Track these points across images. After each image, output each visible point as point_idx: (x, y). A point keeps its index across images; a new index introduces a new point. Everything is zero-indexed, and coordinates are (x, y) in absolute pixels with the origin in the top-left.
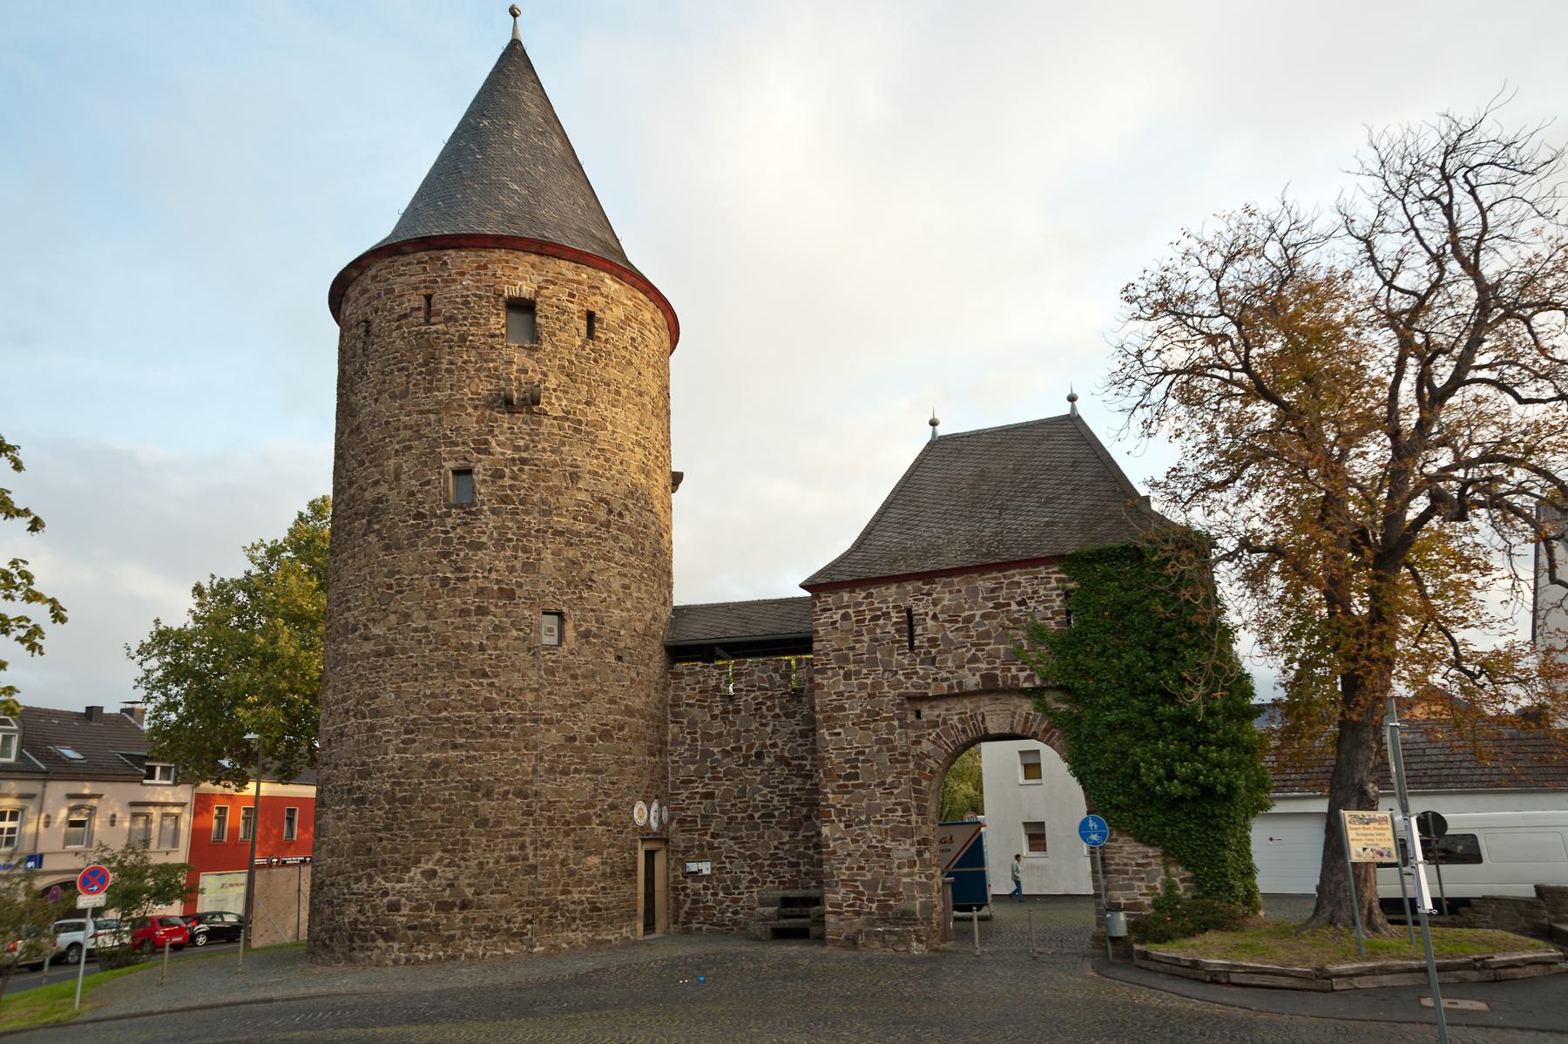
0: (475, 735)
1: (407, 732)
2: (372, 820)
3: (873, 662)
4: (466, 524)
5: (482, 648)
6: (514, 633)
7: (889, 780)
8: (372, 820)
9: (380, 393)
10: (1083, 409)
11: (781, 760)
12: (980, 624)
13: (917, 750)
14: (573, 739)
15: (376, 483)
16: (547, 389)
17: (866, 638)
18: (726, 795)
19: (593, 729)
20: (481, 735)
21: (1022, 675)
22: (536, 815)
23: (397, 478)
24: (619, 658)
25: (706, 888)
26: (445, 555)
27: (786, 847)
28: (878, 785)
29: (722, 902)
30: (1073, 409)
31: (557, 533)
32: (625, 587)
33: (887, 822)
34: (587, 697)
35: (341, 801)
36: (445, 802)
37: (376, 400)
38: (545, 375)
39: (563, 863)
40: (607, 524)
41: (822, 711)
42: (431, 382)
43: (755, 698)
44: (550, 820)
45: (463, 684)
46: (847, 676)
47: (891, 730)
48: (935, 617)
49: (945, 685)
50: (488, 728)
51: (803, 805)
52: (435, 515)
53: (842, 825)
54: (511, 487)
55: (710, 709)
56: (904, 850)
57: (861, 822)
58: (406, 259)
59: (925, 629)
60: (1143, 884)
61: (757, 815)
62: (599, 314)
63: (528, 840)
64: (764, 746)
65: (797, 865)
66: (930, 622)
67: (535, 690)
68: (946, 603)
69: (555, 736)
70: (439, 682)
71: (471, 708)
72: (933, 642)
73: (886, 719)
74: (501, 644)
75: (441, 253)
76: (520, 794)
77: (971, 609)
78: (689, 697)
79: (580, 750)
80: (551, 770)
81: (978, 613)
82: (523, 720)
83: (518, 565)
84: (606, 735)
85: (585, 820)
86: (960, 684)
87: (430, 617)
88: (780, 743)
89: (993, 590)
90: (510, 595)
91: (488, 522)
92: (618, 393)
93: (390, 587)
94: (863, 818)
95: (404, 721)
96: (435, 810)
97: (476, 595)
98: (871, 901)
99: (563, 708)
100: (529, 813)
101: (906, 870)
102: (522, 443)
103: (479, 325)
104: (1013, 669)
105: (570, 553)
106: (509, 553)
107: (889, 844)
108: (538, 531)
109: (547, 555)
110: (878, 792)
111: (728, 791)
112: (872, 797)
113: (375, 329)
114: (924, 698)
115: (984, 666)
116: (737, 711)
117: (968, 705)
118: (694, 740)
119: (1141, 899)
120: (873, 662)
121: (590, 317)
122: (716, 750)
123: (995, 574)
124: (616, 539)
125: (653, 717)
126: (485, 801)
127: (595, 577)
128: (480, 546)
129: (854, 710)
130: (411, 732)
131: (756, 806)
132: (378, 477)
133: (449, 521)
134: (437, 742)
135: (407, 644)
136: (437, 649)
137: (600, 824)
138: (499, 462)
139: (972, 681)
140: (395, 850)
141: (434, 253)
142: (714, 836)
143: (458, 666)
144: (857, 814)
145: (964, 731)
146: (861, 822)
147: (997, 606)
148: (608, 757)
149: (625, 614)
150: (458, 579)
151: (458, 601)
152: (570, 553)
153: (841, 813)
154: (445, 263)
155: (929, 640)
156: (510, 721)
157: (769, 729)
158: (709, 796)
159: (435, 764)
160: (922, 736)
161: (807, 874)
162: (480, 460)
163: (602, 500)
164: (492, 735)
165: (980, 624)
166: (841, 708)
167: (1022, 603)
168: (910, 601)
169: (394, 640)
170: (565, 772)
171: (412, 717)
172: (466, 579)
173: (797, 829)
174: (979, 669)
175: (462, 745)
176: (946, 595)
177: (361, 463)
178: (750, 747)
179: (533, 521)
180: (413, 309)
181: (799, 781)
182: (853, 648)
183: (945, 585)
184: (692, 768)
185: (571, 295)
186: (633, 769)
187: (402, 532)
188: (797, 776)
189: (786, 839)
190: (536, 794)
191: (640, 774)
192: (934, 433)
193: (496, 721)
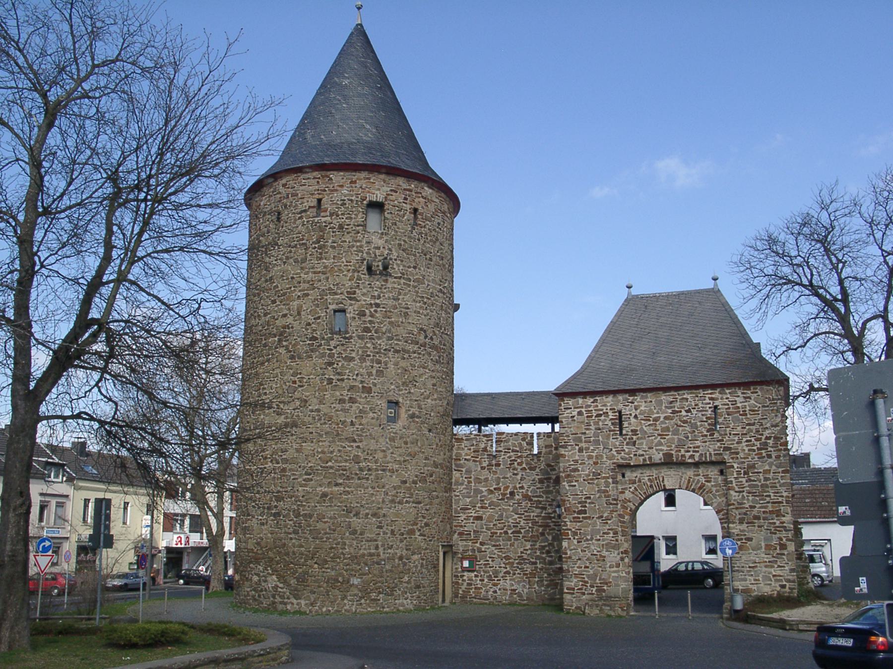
0: (348, 478)
1: (307, 474)
2: (285, 526)
3: (597, 442)
4: (343, 345)
5: (352, 423)
6: (371, 415)
7: (605, 515)
8: (285, 526)
9: (287, 258)
10: (722, 286)
11: (526, 497)
12: (662, 423)
13: (622, 497)
14: (405, 482)
15: (285, 316)
16: (391, 259)
17: (593, 427)
18: (490, 519)
19: (416, 476)
20: (353, 478)
21: (688, 454)
22: (384, 529)
23: (299, 314)
24: (430, 431)
25: (476, 576)
26: (330, 364)
27: (529, 552)
28: (598, 518)
29: (486, 586)
30: (716, 285)
31: (397, 351)
32: (434, 385)
33: (603, 540)
34: (413, 455)
35: (262, 514)
36: (330, 518)
37: (285, 263)
38: (390, 250)
39: (401, 558)
40: (424, 345)
41: (564, 471)
42: (321, 254)
43: (510, 457)
44: (392, 532)
45: (341, 446)
46: (581, 450)
47: (607, 485)
48: (636, 417)
49: (641, 458)
50: (356, 474)
51: (540, 526)
52: (323, 339)
53: (575, 542)
54: (371, 322)
55: (480, 463)
56: (613, 557)
57: (587, 540)
58: (307, 176)
59: (630, 424)
60: (752, 578)
61: (510, 532)
62: (420, 210)
63: (380, 543)
64: (515, 488)
65: (535, 563)
66: (633, 420)
67: (384, 451)
68: (642, 408)
69: (395, 480)
70: (327, 443)
71: (346, 461)
72: (634, 432)
73: (604, 478)
74: (364, 421)
75: (329, 173)
76: (375, 515)
77: (658, 413)
78: (466, 454)
79: (409, 489)
80: (393, 501)
81: (662, 416)
82: (377, 470)
83: (374, 372)
84: (423, 480)
85: (412, 532)
86: (650, 458)
87: (321, 403)
88: (525, 487)
89: (671, 402)
90: (368, 390)
91: (356, 343)
92: (431, 260)
93: (294, 382)
94: (589, 537)
95: (305, 467)
96: (325, 522)
97: (348, 390)
98: (592, 586)
99: (400, 463)
100: (380, 527)
101: (615, 569)
102: (376, 294)
103: (351, 218)
104: (682, 450)
105: (403, 364)
106: (368, 363)
107: (604, 553)
108: (385, 350)
109: (391, 366)
110: (598, 522)
111: (491, 516)
112: (595, 524)
113: (284, 217)
114: (628, 466)
115: (665, 448)
116: (498, 465)
117: (654, 472)
118: (469, 482)
119: (751, 586)
120: (597, 442)
121: (415, 210)
122: (484, 489)
123: (673, 393)
124: (430, 354)
125: (447, 467)
126: (355, 519)
127: (417, 379)
128: (352, 359)
129: (585, 471)
130: (310, 474)
131: (509, 526)
132: (285, 312)
133: (333, 343)
134: (326, 481)
135: (306, 419)
136: (325, 423)
137: (421, 535)
138: (363, 306)
139: (658, 457)
140: (301, 546)
141: (324, 173)
142: (482, 544)
143: (338, 435)
144: (585, 535)
145: (651, 486)
146: (587, 540)
147: (674, 412)
148: (425, 493)
149: (433, 402)
150: (338, 380)
151: (338, 394)
152: (403, 364)
153: (575, 534)
154: (331, 179)
155: (632, 431)
156: (369, 470)
157: (519, 477)
158: (479, 518)
159: (324, 495)
160: (626, 489)
161: (541, 569)
162: (351, 305)
163: (422, 329)
164: (359, 479)
165: (662, 423)
166: (576, 470)
167: (688, 411)
168: (620, 406)
169: (298, 416)
170: (400, 503)
171: (310, 465)
172: (343, 380)
173: (536, 542)
174: (662, 450)
175: (341, 484)
176: (642, 404)
177: (274, 302)
178: (506, 488)
179: (383, 343)
180: (310, 207)
181: (539, 510)
182: (585, 433)
183: (642, 398)
184: (468, 500)
185: (406, 199)
186: (437, 501)
187: (302, 348)
188: (537, 507)
189: (528, 547)
190: (384, 516)
191: (440, 504)
192: (629, 294)
193: (361, 469)
